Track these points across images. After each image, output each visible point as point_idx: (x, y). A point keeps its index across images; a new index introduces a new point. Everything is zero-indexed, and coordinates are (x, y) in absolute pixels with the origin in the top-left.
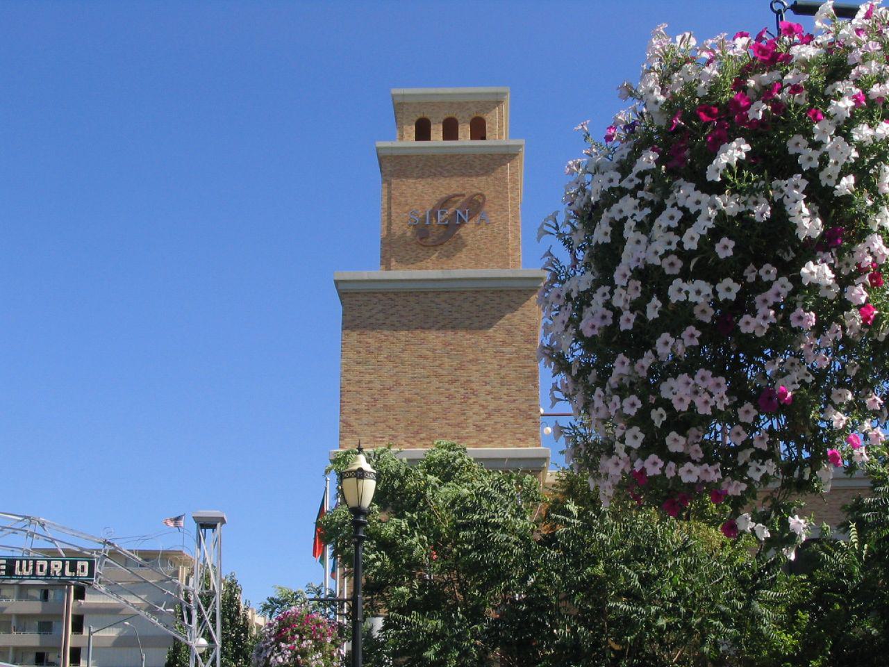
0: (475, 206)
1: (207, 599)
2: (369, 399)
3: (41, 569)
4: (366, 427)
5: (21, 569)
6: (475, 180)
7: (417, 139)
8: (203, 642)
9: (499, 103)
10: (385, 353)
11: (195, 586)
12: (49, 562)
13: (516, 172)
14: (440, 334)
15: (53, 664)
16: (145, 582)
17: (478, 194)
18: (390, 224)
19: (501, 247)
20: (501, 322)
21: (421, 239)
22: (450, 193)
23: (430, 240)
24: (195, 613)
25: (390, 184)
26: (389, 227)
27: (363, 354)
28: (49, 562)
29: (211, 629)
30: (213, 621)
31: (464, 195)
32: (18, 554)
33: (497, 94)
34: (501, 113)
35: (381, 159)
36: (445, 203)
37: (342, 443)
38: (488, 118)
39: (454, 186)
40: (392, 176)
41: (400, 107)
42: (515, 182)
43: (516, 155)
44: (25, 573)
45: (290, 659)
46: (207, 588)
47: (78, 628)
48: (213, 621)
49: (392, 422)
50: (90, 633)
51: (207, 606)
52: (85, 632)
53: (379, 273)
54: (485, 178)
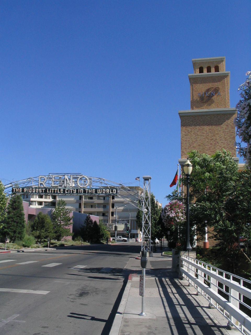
0: (216, 91)
1: (147, 199)
5: (99, 192)
10: (193, 132)
12: (106, 190)
13: (228, 80)
14: (208, 127)
15: (106, 216)
20: (225, 123)
22: (210, 87)
23: (204, 101)
26: (193, 99)
28: (106, 190)
31: (213, 88)
33: (222, 59)
34: (223, 64)
36: (208, 90)
37: (182, 157)
38: (219, 65)
41: (194, 64)
43: (228, 76)
46: (147, 196)
51: (147, 201)
52: (115, 208)
53: (191, 111)
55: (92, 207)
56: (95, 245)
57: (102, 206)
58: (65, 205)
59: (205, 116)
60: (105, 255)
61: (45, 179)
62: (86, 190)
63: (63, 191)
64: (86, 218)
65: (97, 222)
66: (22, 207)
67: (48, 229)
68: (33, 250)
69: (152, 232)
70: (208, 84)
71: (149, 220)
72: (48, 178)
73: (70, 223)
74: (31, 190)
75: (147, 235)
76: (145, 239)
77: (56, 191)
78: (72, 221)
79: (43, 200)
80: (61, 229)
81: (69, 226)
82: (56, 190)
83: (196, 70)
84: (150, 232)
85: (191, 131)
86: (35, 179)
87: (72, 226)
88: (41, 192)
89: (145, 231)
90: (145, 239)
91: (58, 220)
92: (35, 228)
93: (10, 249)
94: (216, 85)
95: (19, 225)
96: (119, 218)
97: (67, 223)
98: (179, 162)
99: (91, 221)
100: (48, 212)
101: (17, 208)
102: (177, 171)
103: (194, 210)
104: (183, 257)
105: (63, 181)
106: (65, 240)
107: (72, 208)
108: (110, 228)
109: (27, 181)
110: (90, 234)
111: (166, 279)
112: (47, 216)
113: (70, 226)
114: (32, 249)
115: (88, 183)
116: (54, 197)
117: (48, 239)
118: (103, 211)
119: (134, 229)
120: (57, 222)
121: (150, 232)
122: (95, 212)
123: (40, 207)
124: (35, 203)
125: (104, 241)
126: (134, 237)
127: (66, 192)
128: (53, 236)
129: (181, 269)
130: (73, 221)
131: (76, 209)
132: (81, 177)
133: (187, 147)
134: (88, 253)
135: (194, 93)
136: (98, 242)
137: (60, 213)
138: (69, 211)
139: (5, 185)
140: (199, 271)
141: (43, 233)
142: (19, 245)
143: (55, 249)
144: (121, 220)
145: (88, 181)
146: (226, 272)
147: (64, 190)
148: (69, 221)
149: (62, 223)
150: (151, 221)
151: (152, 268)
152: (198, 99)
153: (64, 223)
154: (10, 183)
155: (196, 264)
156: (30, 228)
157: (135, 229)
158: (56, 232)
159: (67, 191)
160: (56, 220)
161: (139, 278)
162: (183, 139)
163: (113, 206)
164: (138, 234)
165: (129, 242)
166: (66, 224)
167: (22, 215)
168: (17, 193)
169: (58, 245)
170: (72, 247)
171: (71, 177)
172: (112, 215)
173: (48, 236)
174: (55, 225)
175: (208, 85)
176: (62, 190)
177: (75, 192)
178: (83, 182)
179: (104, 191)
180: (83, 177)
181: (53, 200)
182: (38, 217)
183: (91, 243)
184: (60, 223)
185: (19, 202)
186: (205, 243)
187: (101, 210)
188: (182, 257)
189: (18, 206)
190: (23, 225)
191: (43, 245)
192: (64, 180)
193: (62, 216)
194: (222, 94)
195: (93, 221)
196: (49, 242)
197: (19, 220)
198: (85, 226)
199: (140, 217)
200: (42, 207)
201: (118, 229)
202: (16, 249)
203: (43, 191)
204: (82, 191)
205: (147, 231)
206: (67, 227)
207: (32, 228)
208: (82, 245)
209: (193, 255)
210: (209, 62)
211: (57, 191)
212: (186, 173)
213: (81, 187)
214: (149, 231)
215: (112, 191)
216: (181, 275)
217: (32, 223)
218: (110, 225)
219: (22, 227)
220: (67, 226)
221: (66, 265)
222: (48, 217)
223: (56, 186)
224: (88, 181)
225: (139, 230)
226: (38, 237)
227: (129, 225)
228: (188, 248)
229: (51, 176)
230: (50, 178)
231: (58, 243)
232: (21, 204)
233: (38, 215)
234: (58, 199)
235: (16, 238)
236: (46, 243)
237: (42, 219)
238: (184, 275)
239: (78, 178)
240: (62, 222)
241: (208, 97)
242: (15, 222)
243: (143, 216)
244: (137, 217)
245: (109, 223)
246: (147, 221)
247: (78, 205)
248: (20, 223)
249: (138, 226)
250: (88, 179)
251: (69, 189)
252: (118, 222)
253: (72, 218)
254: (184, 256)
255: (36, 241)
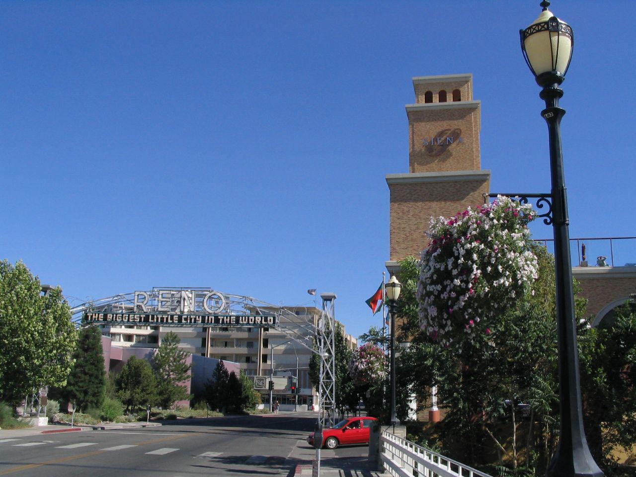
0: (456, 135)
1: (328, 334)
2: (403, 236)
3: (252, 321)
4: (403, 250)
5: (242, 321)
6: (456, 122)
7: (426, 102)
8: (327, 354)
9: (467, 82)
10: (411, 213)
11: (322, 327)
12: (255, 317)
13: (477, 117)
14: (438, 203)
15: (254, 362)
16: (299, 326)
17: (457, 129)
18: (414, 145)
19: (470, 155)
20: (468, 197)
21: (429, 153)
22: (443, 129)
23: (434, 153)
24: (322, 341)
25: (413, 126)
26: (413, 148)
27: (401, 214)
28: (255, 317)
29: (330, 347)
30: (331, 344)
31: (450, 130)
32: (240, 314)
33: (466, 77)
34: (468, 86)
35: (408, 113)
36: (441, 134)
37: (391, 257)
38: (461, 89)
39: (445, 125)
40: (414, 121)
41: (417, 86)
42: (476, 122)
43: (477, 108)
44: (244, 322)
45: (366, 366)
46: (328, 329)
47: (266, 345)
48: (331, 344)
49: (415, 247)
50: (272, 348)
51: (328, 337)
52: (269, 347)
53: (408, 174)
54: (461, 120)
55: (226, 345)
56: (232, 417)
57: (246, 342)
58: (178, 342)
59: (433, 185)
60: (254, 434)
61: (145, 298)
62: (219, 317)
63: (177, 319)
64: (216, 367)
65: (235, 374)
66: (101, 348)
67: (147, 387)
68: (120, 426)
69: (336, 393)
70: (440, 123)
71: (332, 371)
72: (151, 295)
73: (186, 376)
74: (120, 318)
75: (329, 399)
76: (324, 406)
77: (165, 320)
78: (189, 372)
79: (134, 331)
80: (171, 388)
81: (184, 382)
82: (165, 317)
83: (419, 96)
84: (334, 393)
85: (408, 211)
86: (128, 297)
87: (190, 382)
88: (138, 320)
89: (324, 392)
90: (324, 406)
91: (164, 370)
92: (123, 385)
93: (79, 425)
94: (455, 124)
95: (93, 379)
96: (277, 366)
97: (181, 377)
98: (387, 267)
99: (226, 372)
100: (146, 355)
101: (90, 348)
102: (381, 286)
103: (406, 358)
104: (385, 436)
105: (179, 302)
106: (176, 408)
107: (189, 346)
108: (260, 385)
109: (112, 301)
110: (224, 396)
111: (357, 472)
112: (144, 364)
113: (186, 381)
114: (118, 425)
115: (223, 304)
116: (156, 328)
117: (147, 406)
118: (247, 353)
119: (305, 387)
120: (162, 373)
121: (334, 393)
122: (232, 355)
123: (128, 344)
124: (118, 337)
125: (249, 410)
126: (305, 403)
127: (183, 321)
128: (157, 399)
129: (381, 455)
130: (192, 372)
131: (197, 349)
132: (210, 294)
133: (401, 240)
134: (221, 432)
135: (415, 139)
136: (238, 411)
137: (169, 357)
138: (185, 353)
139: (73, 308)
140: (419, 465)
141: (137, 395)
142: (93, 416)
143: (160, 425)
144: (281, 371)
145: (224, 301)
146: (463, 466)
147: (180, 318)
148: (186, 371)
149: (172, 376)
150: (336, 373)
151: (336, 457)
152: (423, 150)
153: (175, 376)
154: (82, 305)
155: (414, 453)
156: (114, 386)
157: (307, 386)
158: (161, 393)
159: (186, 319)
160: (162, 371)
161: (312, 470)
162: (395, 225)
163: (266, 345)
164: (312, 396)
165: (296, 411)
166: (180, 378)
167: (102, 360)
168: (93, 322)
169: (165, 416)
170: (191, 421)
171: (193, 293)
172: (265, 360)
173: (147, 400)
174: (159, 380)
175: (440, 124)
176: (176, 318)
177: (199, 322)
178: (213, 302)
179: (251, 319)
180: (215, 295)
181: (153, 332)
182: (129, 365)
183: (226, 413)
184: (169, 375)
185: (94, 337)
186: (431, 414)
187: (244, 350)
188: (383, 436)
189: (93, 345)
190: (101, 380)
191: (138, 418)
192: (179, 300)
193: (171, 364)
194: (465, 140)
195: (229, 373)
196: (148, 412)
197: (95, 370)
198: (213, 382)
199: (315, 366)
200: (131, 346)
201: (276, 387)
202: (90, 425)
203: (143, 319)
204: (211, 319)
205: (328, 392)
206: (180, 384)
207: (116, 385)
208: (209, 417)
209: (402, 432)
210: (443, 84)
211: (167, 318)
212: (390, 297)
213: (211, 312)
214: (331, 391)
215: (266, 320)
216: (382, 465)
217: (117, 376)
218: (260, 380)
219: (100, 383)
220: (180, 381)
221: (186, 452)
222: (146, 365)
223: (166, 309)
224: (224, 301)
225: (314, 389)
226: (128, 402)
227: (295, 380)
228: (392, 420)
229: (157, 293)
230: (155, 296)
231: (165, 413)
232: (99, 340)
233: (128, 361)
234: (161, 329)
235: (89, 404)
236: (142, 414)
237: (137, 368)
238: (386, 466)
239: (205, 295)
240: (171, 373)
241: (441, 147)
242: (86, 374)
243: (322, 365)
244: (310, 365)
245: (259, 375)
246: (327, 373)
247: (200, 341)
248: (95, 376)
249: (312, 383)
250: (222, 298)
251: (189, 317)
252: (275, 374)
253: (190, 367)
254: (386, 434)
255: (124, 409)
